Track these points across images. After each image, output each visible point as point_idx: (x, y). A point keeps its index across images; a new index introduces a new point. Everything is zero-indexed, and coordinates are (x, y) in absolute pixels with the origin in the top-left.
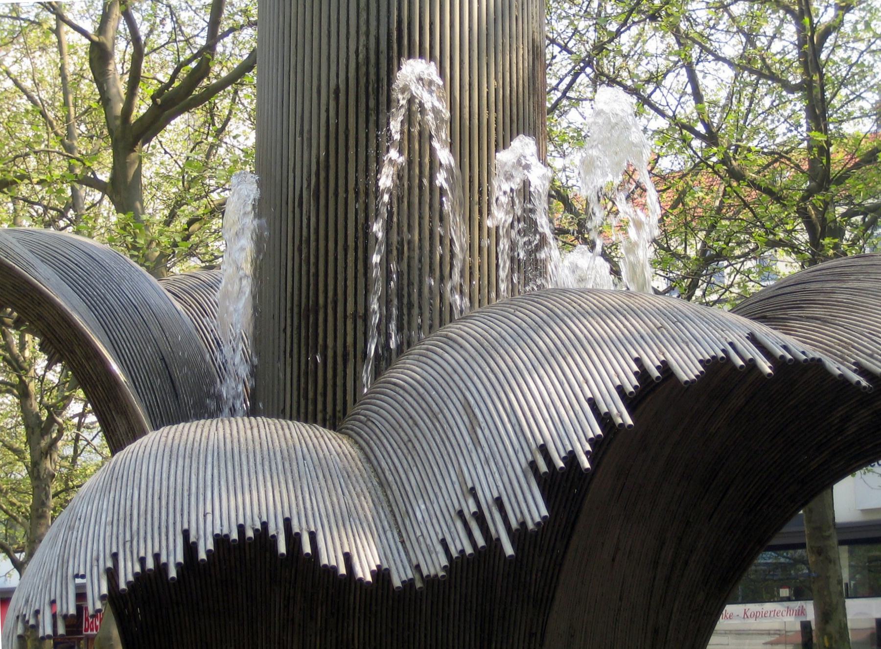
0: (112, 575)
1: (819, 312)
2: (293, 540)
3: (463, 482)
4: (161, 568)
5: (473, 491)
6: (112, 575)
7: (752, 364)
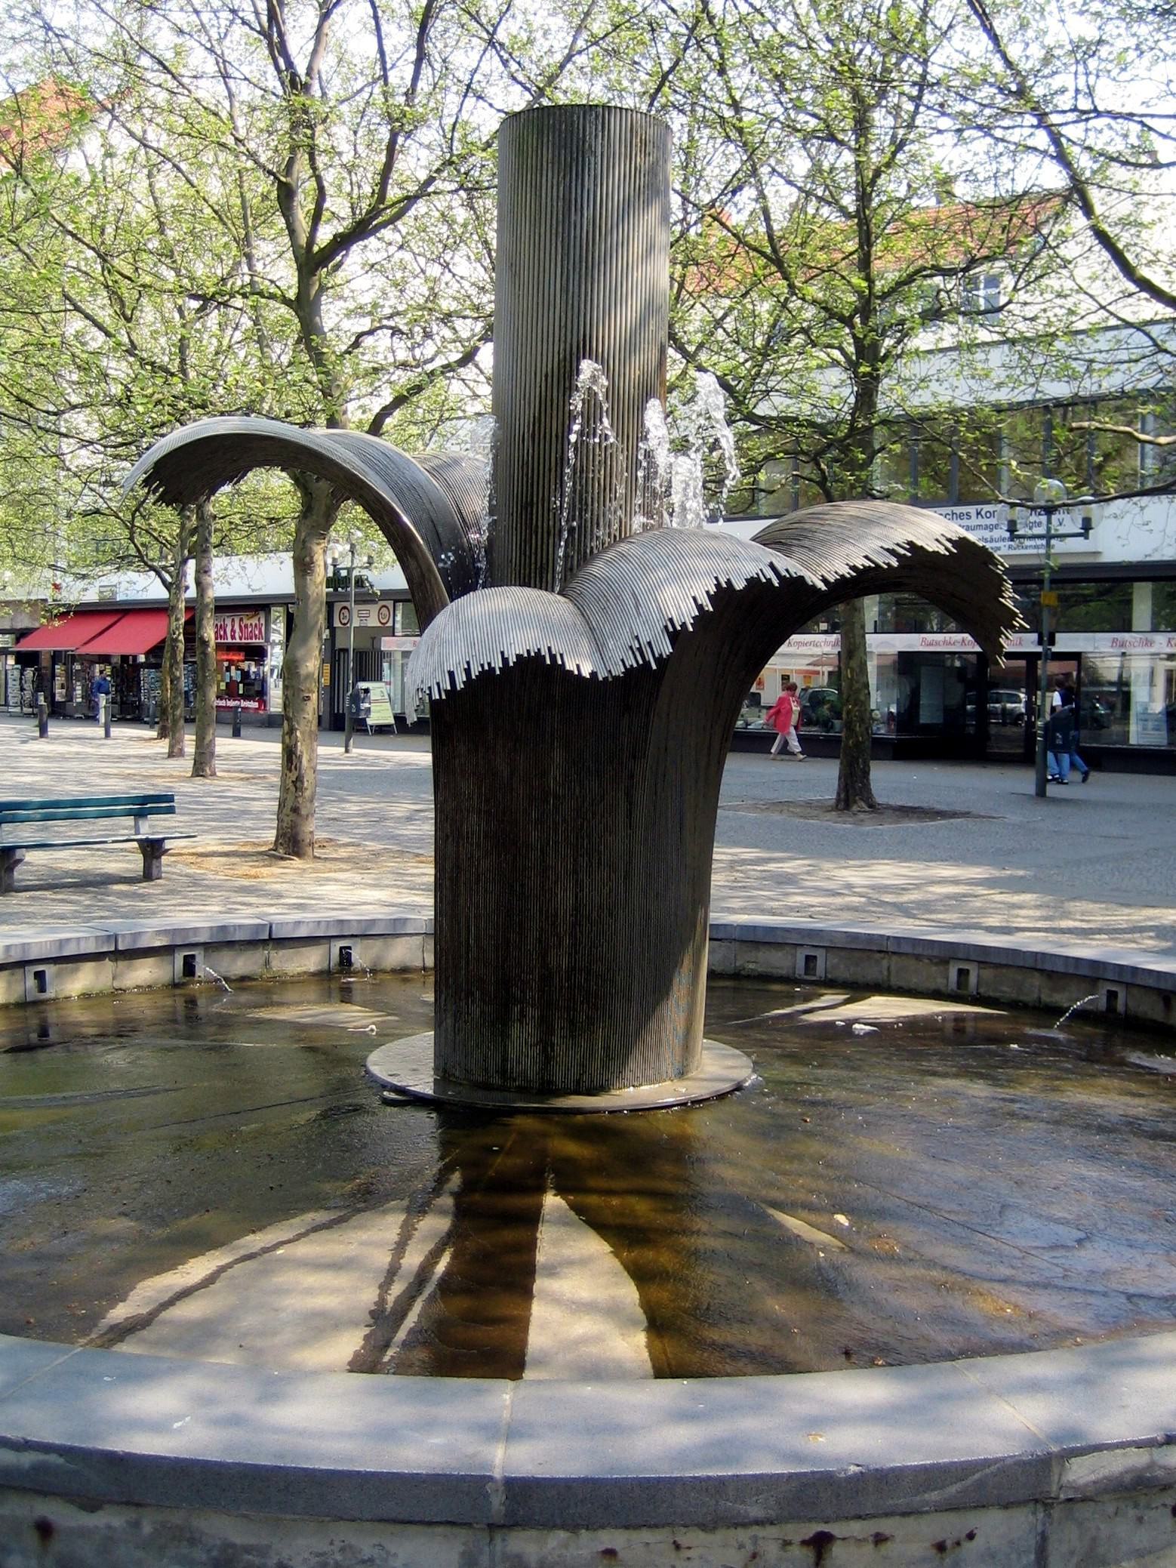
0: (468, 671)
1: (806, 543)
2: (553, 657)
3: (632, 633)
4: (492, 670)
5: (637, 637)
6: (468, 671)
7: (769, 580)
